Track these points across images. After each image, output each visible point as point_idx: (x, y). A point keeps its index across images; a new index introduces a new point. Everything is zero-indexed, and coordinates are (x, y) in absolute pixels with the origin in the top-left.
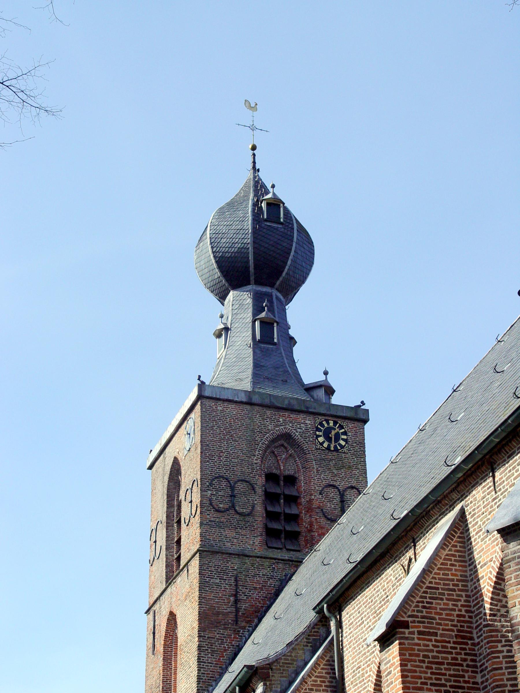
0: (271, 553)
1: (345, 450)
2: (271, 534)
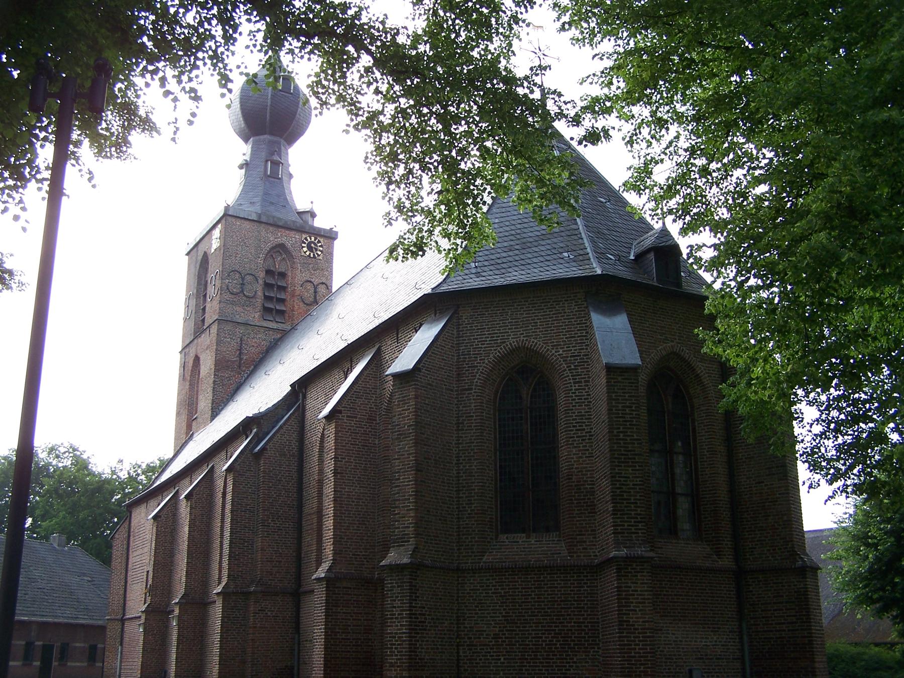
0: (265, 324)
1: (320, 258)
2: (267, 310)
